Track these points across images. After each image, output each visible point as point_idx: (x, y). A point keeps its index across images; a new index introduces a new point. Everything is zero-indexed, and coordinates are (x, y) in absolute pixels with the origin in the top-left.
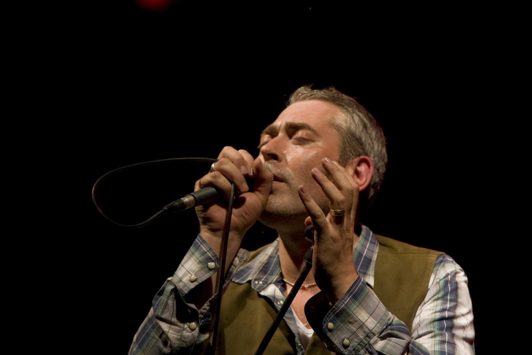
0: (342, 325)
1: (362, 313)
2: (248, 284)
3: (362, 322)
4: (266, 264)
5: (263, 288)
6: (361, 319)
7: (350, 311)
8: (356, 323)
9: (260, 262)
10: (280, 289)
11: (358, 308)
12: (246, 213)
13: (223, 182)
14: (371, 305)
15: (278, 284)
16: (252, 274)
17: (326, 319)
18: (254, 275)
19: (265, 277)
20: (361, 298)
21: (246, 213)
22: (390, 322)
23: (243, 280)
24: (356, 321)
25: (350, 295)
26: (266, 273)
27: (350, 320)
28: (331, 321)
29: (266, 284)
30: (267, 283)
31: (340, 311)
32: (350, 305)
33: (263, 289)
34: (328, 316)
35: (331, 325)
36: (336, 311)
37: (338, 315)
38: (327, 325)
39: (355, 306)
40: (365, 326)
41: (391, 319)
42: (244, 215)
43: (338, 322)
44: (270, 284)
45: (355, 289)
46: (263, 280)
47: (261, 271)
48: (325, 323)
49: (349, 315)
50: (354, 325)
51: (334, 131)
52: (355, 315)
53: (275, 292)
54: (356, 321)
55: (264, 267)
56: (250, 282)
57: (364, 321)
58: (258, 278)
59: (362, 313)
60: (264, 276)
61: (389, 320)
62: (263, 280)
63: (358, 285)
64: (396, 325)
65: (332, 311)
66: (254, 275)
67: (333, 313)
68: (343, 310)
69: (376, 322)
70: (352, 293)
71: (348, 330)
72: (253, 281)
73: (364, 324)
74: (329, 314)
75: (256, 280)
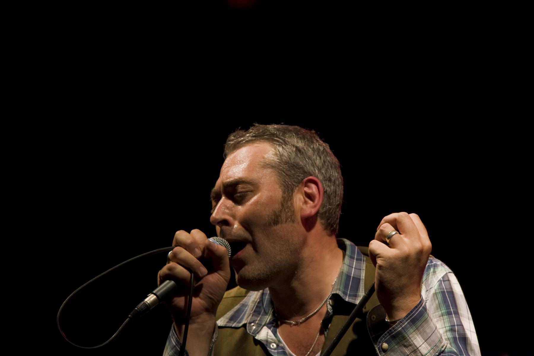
0: (396, 347)
1: (418, 338)
2: (242, 329)
3: (416, 346)
4: (259, 302)
5: (258, 332)
6: (416, 343)
7: (406, 335)
8: (410, 347)
9: (253, 301)
10: (272, 331)
11: (414, 333)
12: (211, 294)
13: (180, 270)
14: (428, 331)
15: (270, 326)
16: (245, 317)
17: (382, 339)
18: (248, 317)
19: (259, 319)
20: (419, 323)
21: (211, 294)
22: (443, 349)
23: (239, 322)
24: (411, 345)
25: (409, 319)
26: (259, 314)
27: (405, 344)
28: (386, 342)
29: (260, 326)
30: (261, 325)
31: (396, 334)
32: (407, 329)
33: (258, 333)
34: (384, 337)
35: (385, 345)
36: (392, 333)
37: (394, 337)
38: (382, 345)
39: (412, 330)
40: (419, 350)
41: (445, 347)
42: (210, 296)
43: (393, 344)
44: (264, 326)
45: (415, 313)
46: (257, 322)
47: (254, 311)
48: (380, 342)
49: (404, 338)
50: (409, 348)
51: (269, 170)
52: (410, 339)
53: (267, 335)
54: (411, 345)
55: (257, 306)
56: (245, 326)
57: (418, 346)
58: (252, 321)
59: (418, 338)
60: (258, 317)
61: (442, 347)
62: (257, 322)
63: (418, 309)
64: (448, 352)
65: (388, 332)
66: (248, 317)
67: (389, 334)
68: (400, 333)
69: (430, 348)
70: (411, 317)
71: (402, 352)
72: (248, 325)
73: (418, 348)
74: (386, 334)
75: (250, 323)
